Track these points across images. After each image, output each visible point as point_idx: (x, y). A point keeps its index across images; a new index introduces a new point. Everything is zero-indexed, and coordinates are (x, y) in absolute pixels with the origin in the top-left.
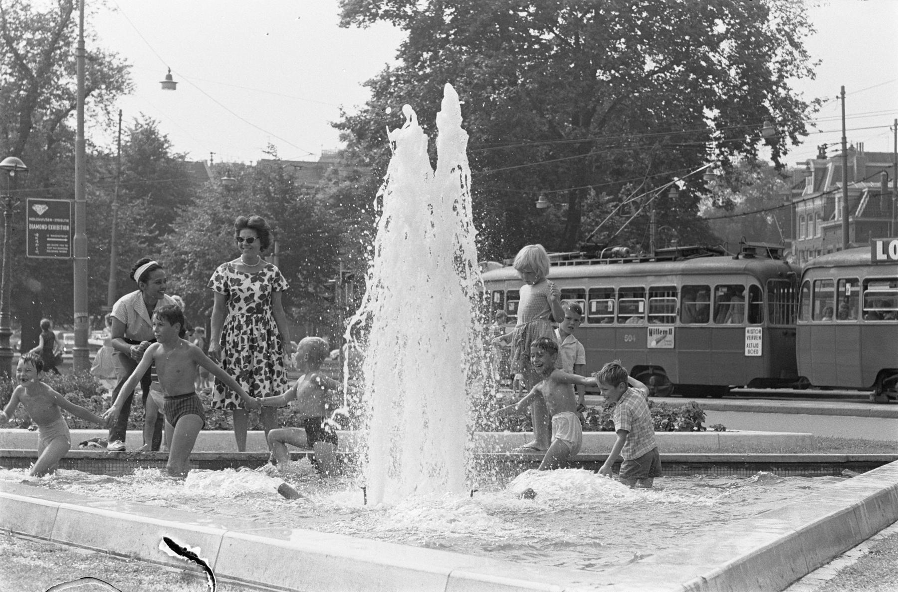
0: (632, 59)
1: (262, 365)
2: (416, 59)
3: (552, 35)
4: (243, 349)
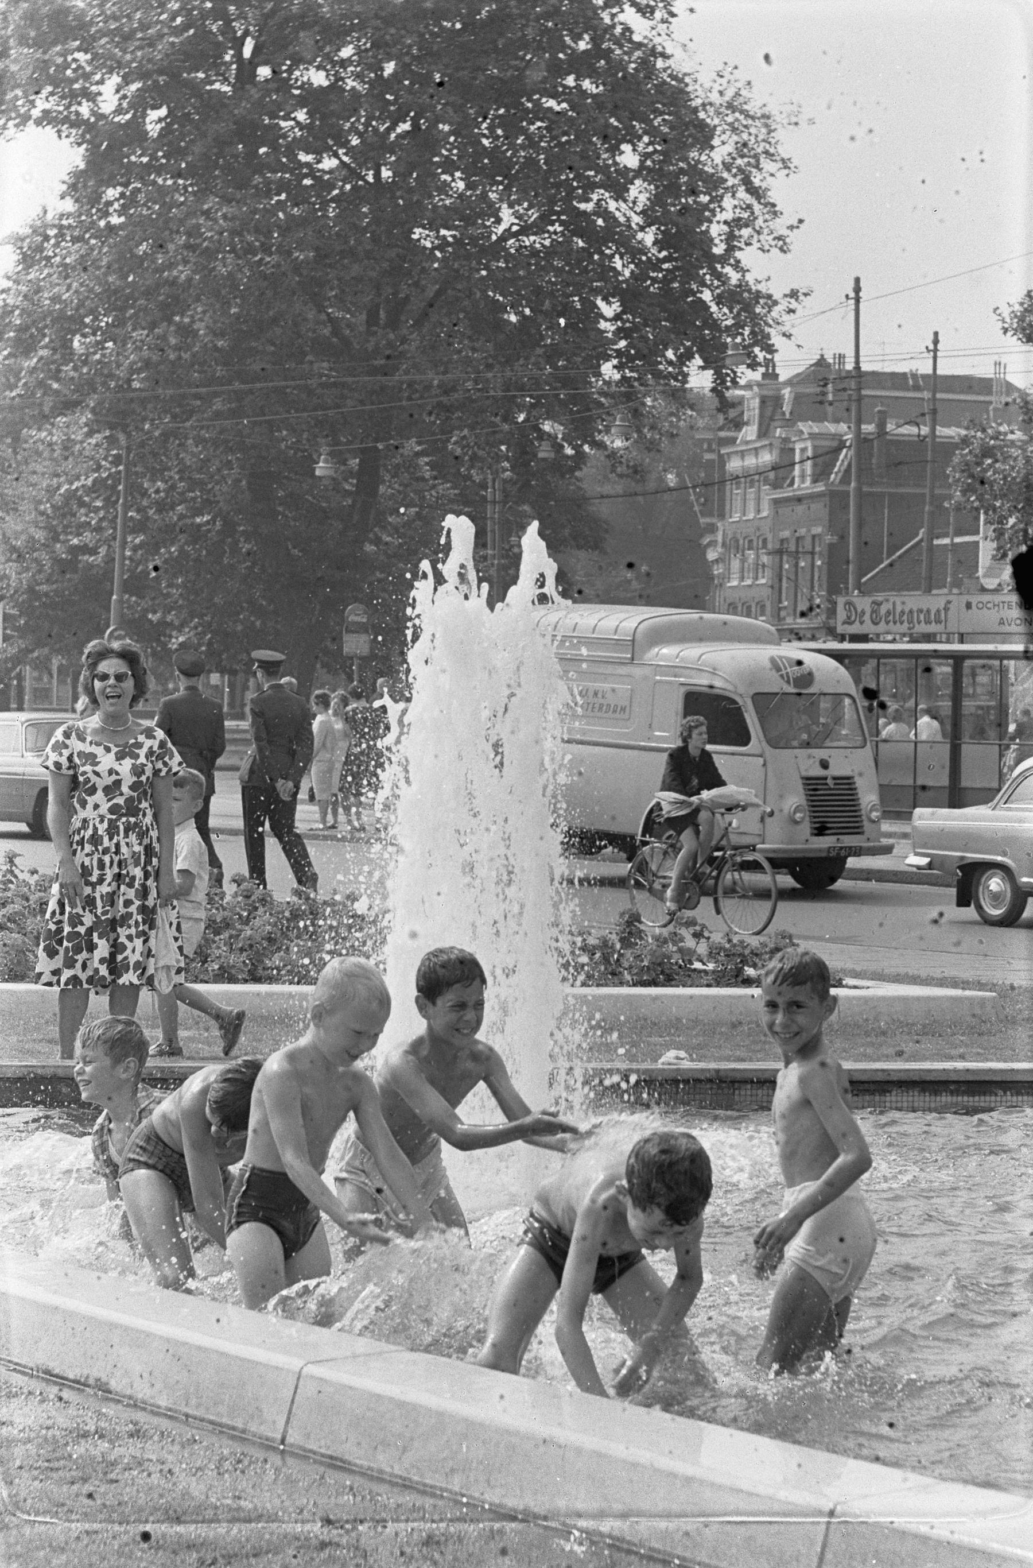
0: (473, 212)
1: (133, 909)
2: (95, 198)
3: (334, 163)
4: (101, 880)
